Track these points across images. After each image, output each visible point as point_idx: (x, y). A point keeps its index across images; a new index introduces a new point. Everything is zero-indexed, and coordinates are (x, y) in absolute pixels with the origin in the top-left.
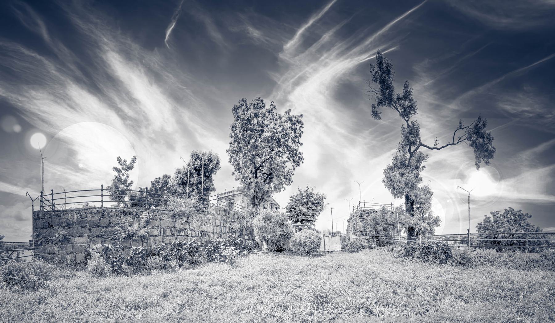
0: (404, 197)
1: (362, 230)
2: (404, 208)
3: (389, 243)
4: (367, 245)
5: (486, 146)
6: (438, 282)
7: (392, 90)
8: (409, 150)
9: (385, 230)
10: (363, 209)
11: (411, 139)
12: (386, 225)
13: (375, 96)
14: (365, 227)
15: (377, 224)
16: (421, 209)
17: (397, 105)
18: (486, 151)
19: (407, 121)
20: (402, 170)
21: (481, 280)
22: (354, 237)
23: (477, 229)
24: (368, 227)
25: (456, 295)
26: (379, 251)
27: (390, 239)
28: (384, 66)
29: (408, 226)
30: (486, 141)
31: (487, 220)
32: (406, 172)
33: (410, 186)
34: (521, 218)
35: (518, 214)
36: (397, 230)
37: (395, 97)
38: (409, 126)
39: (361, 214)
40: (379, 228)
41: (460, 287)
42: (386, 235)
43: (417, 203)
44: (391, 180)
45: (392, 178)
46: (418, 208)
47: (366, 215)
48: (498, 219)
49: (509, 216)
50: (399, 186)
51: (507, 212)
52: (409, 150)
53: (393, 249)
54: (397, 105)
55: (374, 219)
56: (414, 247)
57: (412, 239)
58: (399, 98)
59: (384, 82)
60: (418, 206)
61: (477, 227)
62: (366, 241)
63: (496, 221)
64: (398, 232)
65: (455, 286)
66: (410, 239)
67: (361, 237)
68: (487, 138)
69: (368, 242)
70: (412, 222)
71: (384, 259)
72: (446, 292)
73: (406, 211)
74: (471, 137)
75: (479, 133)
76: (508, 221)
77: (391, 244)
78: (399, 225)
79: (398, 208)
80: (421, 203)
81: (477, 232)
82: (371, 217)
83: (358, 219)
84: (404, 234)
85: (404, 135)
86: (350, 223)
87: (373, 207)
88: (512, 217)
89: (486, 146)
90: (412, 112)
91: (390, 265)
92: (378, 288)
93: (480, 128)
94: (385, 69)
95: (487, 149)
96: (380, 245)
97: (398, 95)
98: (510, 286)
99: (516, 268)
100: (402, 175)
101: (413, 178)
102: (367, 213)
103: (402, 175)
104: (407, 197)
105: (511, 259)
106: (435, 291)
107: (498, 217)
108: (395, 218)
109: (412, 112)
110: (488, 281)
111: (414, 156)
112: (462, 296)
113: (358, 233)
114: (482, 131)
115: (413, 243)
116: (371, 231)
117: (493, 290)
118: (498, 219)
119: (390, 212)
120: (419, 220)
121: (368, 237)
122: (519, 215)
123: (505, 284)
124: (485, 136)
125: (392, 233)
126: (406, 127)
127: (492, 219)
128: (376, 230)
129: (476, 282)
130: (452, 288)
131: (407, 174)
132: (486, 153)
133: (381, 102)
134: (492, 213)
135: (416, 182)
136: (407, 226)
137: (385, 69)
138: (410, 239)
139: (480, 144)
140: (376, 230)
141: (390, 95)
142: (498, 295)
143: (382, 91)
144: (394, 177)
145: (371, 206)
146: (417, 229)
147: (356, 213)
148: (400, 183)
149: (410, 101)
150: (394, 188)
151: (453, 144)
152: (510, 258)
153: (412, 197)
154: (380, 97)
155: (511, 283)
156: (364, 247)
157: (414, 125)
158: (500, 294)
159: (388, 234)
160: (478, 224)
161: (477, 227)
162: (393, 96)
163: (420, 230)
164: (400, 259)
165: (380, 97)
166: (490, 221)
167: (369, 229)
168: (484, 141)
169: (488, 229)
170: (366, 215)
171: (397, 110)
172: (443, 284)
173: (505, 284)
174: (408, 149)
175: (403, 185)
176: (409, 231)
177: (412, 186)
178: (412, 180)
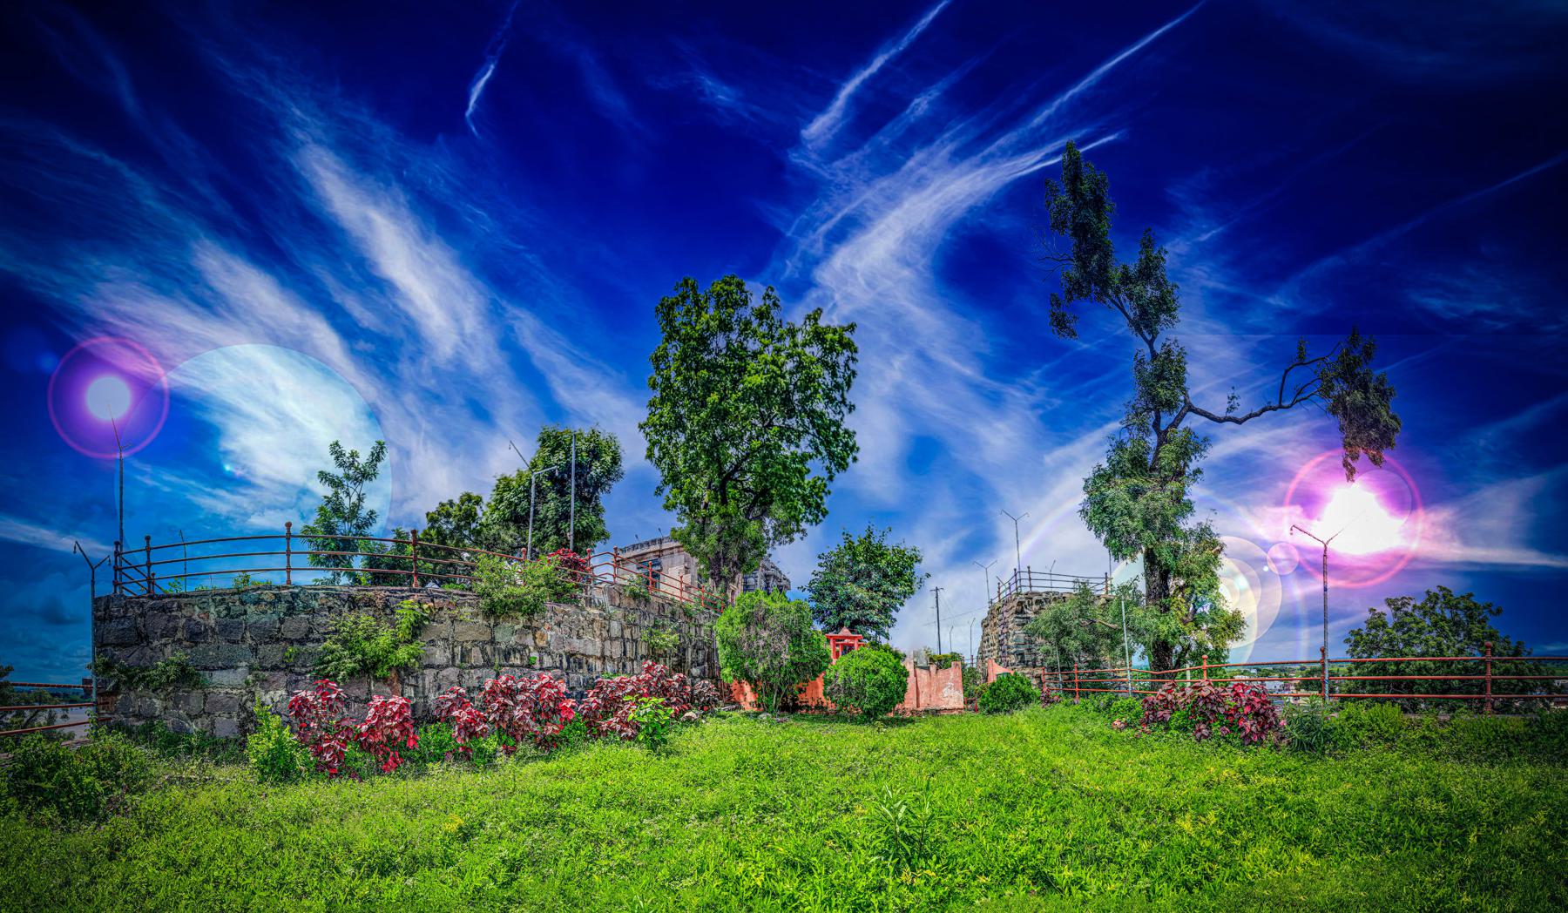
0: (1140, 556)
1: (1022, 649)
2: (1142, 587)
3: (1099, 687)
4: (1038, 692)
8: (1156, 425)
9: (1087, 648)
10: (1024, 590)
12: (1091, 637)
14: (1031, 642)
15: (1065, 632)
16: (1188, 591)
18: (1372, 426)
22: (1000, 670)
23: (1347, 647)
24: (1040, 640)
26: (1069, 713)
27: (1102, 676)
30: (1374, 400)
32: (1147, 485)
36: (1123, 649)
38: (1154, 356)
41: (1299, 812)
42: (1090, 665)
43: (1179, 574)
45: (1108, 503)
46: (1181, 589)
48: (1408, 619)
52: (1156, 425)
53: (1109, 705)
54: (1122, 296)
56: (1170, 697)
57: (1163, 676)
58: (1129, 278)
60: (1182, 583)
62: (1034, 681)
63: (1400, 626)
64: (1123, 656)
65: (1287, 809)
66: (1158, 677)
68: (1377, 390)
69: (1041, 684)
70: (1164, 628)
72: (1260, 826)
73: (1148, 596)
74: (1331, 388)
76: (1435, 624)
77: (1106, 688)
78: (1126, 638)
79: (1124, 589)
82: (1047, 614)
84: (1140, 660)
86: (988, 630)
88: (1448, 614)
90: (1163, 317)
93: (1357, 364)
94: (1089, 197)
95: (1377, 421)
96: (1073, 693)
98: (1441, 808)
99: (1458, 756)
100: (1136, 493)
102: (1038, 602)
103: (1136, 493)
104: (1150, 557)
107: (1406, 614)
109: (1163, 317)
110: (1377, 796)
111: (1169, 442)
112: (1306, 838)
113: (1013, 659)
116: (1047, 653)
118: (1408, 619)
119: (1103, 601)
121: (1039, 671)
123: (1427, 802)
126: (1148, 358)
127: (1390, 620)
128: (1062, 651)
130: (1278, 814)
134: (1390, 602)
135: (1175, 515)
136: (1150, 638)
138: (1158, 677)
139: (1356, 408)
143: (1079, 258)
144: (1112, 499)
153: (1165, 556)
156: (1027, 698)
157: (1168, 352)
158: (1412, 832)
159: (1099, 662)
161: (1347, 641)
163: (1186, 649)
164: (1129, 732)
166: (1384, 625)
168: (1367, 398)
169: (1378, 648)
172: (1250, 804)
173: (1426, 804)
174: (1151, 421)
176: (1156, 653)
177: (1163, 525)
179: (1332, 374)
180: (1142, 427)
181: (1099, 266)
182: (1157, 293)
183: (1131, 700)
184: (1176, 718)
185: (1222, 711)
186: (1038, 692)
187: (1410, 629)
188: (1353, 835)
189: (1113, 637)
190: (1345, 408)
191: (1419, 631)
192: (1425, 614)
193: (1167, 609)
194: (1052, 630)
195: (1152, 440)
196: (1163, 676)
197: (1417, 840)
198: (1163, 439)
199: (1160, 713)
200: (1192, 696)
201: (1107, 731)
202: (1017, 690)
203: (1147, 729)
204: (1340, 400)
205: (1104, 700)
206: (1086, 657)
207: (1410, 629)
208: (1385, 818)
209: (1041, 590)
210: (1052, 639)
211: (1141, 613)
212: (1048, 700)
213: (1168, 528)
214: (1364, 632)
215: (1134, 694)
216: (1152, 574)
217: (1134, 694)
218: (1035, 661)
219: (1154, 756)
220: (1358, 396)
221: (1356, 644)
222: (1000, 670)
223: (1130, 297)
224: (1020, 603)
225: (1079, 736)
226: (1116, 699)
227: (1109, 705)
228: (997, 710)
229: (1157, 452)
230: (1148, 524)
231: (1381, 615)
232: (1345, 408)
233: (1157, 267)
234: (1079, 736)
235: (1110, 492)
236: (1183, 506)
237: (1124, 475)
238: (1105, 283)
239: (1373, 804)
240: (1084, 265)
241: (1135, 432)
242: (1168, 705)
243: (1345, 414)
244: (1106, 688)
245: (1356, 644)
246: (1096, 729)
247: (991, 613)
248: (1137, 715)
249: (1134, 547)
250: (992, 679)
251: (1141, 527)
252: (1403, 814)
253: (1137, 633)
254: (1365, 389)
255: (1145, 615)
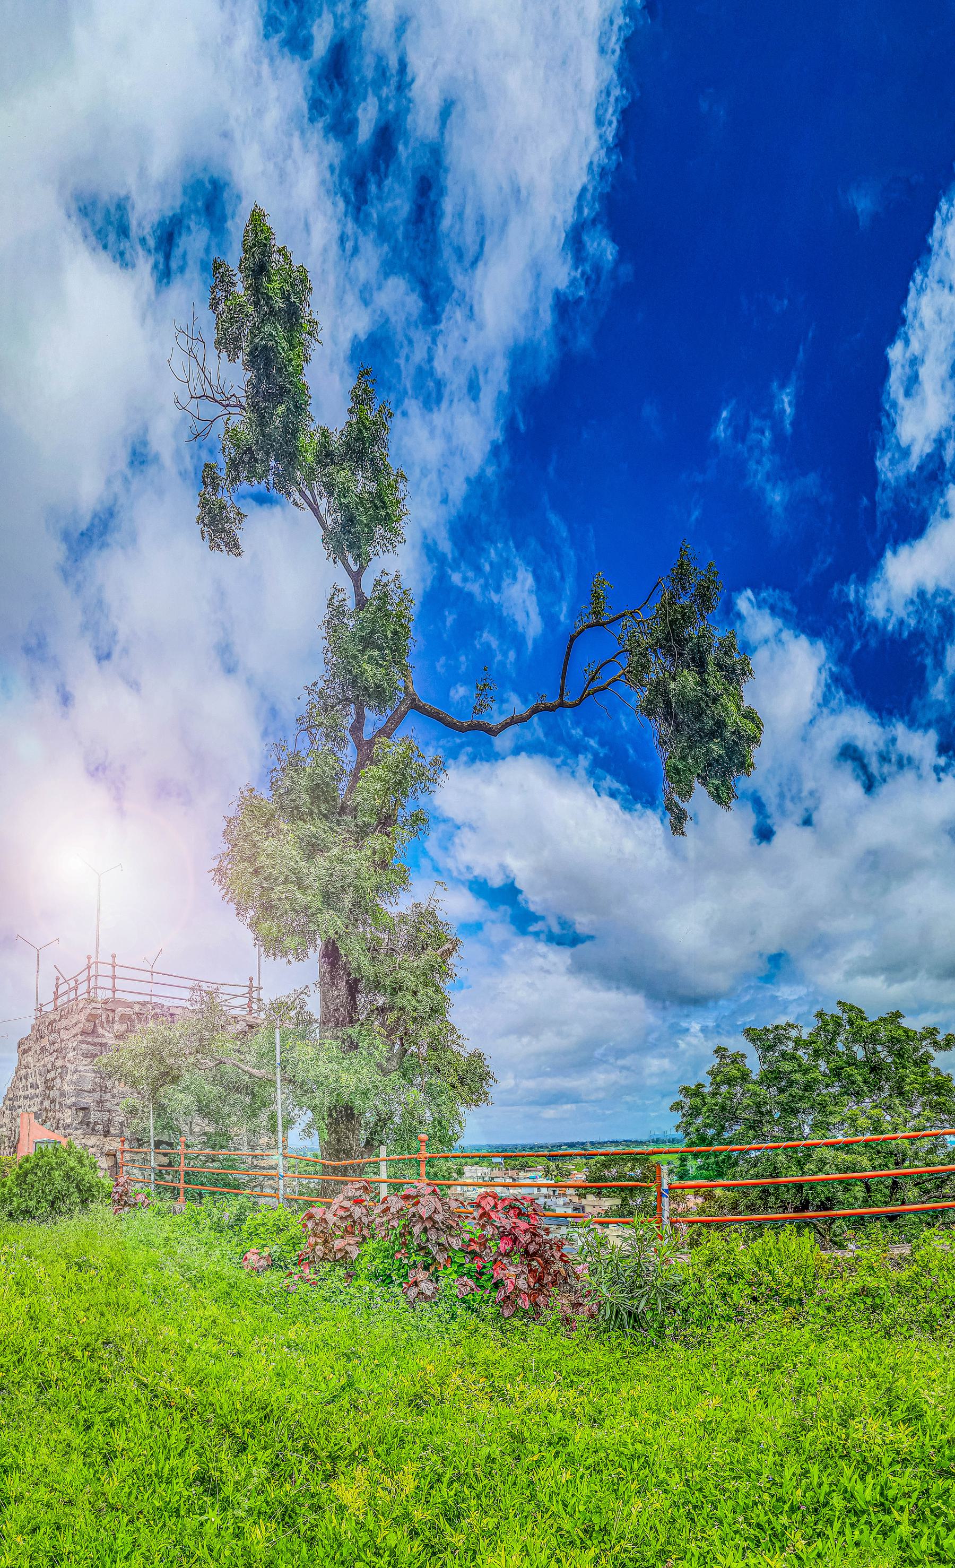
0: (315, 954)
1: (87, 1100)
2: (314, 1006)
3: (225, 1185)
4: (108, 1182)
5: (717, 710)
6: (470, 1429)
7: (299, 408)
8: (357, 729)
9: (205, 1111)
10: (102, 995)
11: (369, 670)
12: (216, 1090)
13: (219, 428)
14: (105, 1090)
15: (169, 1076)
16: (392, 1017)
17: (317, 486)
18: (712, 734)
19: (356, 578)
20: (314, 828)
21: (738, 1411)
22: (42, 1133)
23: (677, 1117)
24: (121, 1088)
25: (567, 1524)
26: (167, 1226)
27: (231, 1164)
28: (274, 286)
29: (327, 1101)
30: (716, 684)
31: (728, 1072)
32: (331, 838)
33: (347, 902)
34: (900, 1055)
35: (883, 1036)
36: (273, 1117)
37: (309, 445)
38: (361, 602)
39: (92, 1018)
40: (179, 1100)
41: (596, 1469)
42: (211, 1141)
43: (377, 985)
44: (256, 872)
45: (262, 860)
46: (382, 1011)
47: (119, 1027)
48: (786, 1066)
49: (840, 1047)
50: (293, 901)
51: (829, 1027)
52: (357, 729)
53: (239, 1219)
54: (317, 486)
55: (155, 1053)
56: (358, 1212)
57: (345, 1171)
58: (329, 454)
59: (268, 363)
60: (380, 1001)
61: (677, 1107)
62: (104, 1163)
63: (773, 1077)
64: (273, 1129)
65: (571, 1460)
66: (336, 1171)
67: (79, 1140)
68: (720, 666)
69: (116, 1168)
70: (348, 1079)
71: (185, 1269)
72: (512, 1500)
73: (324, 1022)
74: (645, 667)
75: (681, 642)
76: (837, 1072)
77: (236, 1187)
78: (280, 1095)
79: (280, 1008)
80: (397, 989)
81: (680, 1134)
82: (137, 1042)
83: (71, 1040)
84: (303, 1139)
85: (338, 648)
86: (29, 1059)
87: (158, 990)
88: (859, 1053)
89: (717, 710)
90: (379, 531)
91: (213, 1310)
92: (119, 1440)
93: (686, 619)
94: (279, 303)
95: (720, 725)
96: (175, 1193)
97: (325, 434)
98: (904, 1438)
99: (929, 1325)
100: (313, 848)
101: (365, 867)
102: (124, 1018)
103: (313, 848)
104: (332, 954)
105: (904, 1275)
106: (444, 1493)
107: (784, 1055)
108: (266, 1055)
109: (379, 531)
110: (773, 1420)
111: (375, 762)
112: (605, 1531)
113: (68, 1117)
114: (692, 632)
115: (351, 1190)
116: (133, 1111)
117: (805, 1473)
118: (786, 1066)
119: (242, 1026)
120: (386, 1073)
121: (114, 1145)
122: (893, 1040)
123: (874, 1426)
124: (711, 658)
125: (240, 1131)
126: (350, 604)
127: (754, 1064)
128: (161, 1110)
129: (709, 1428)
130: (554, 1473)
131: (335, 851)
132: (716, 749)
133: (244, 461)
134: (753, 1035)
135: (377, 888)
136: (323, 1099)
137: (279, 303)
138: (336, 1171)
139: (686, 704)
140: (161, 1110)
141: (291, 432)
142: (837, 1501)
143: (255, 407)
144: (271, 856)
145: (146, 988)
146: (370, 1117)
147: (66, 1015)
148: (300, 884)
149: (378, 470)
150: (267, 908)
151: (562, 705)
152: (894, 1274)
153: (356, 955)
154: (248, 436)
155: (907, 1421)
156: (86, 1195)
157: (384, 598)
158: (848, 1495)
159: (224, 1135)
160: (685, 1091)
161: (677, 1107)
162: (303, 440)
163: (383, 1121)
164: (273, 1277)
165: (248, 436)
166: (745, 1077)
167: (124, 1098)
168: (704, 683)
169: (735, 1119)
170: (119, 1027)
171: (316, 511)
172: (495, 1450)
173: (872, 1431)
174: (349, 721)
175: (312, 898)
176: (333, 1126)
177: (356, 904)
178: (358, 875)
179: (646, 640)
180: (333, 732)
181: (286, 427)
182: (373, 487)
183: (282, 1212)
184: (368, 1256)
185: (456, 1243)
186: (108, 1182)
187: (791, 1084)
188: (725, 1510)
189: (254, 1095)
190: (668, 704)
191: (808, 1088)
192: (817, 1054)
193: (354, 1046)
194: (146, 1071)
195: (349, 755)
196: (345, 1171)
197: (858, 1513)
198: (366, 756)
199: (338, 1244)
200: (400, 1214)
201: (229, 1271)
202: (67, 1177)
203: (309, 1273)
204: (660, 688)
205: (231, 1209)
206: (202, 1126)
207: (791, 1084)
208: (792, 1468)
209: (131, 998)
210: (145, 1087)
211: (311, 1052)
212: (122, 1201)
213: (363, 909)
214: (707, 1090)
215: (289, 1201)
216: (333, 984)
217: (289, 1201)
218: (109, 1123)
219: (317, 1333)
220: (690, 678)
221: (695, 1112)
222: (42, 1133)
223: (330, 488)
224: (92, 1018)
225: (171, 1276)
226: (255, 1208)
227: (239, 1219)
228: (27, 1213)
229: (356, 778)
230: (329, 899)
231: (737, 1059)
232: (668, 704)
233: (375, 440)
234: (171, 1276)
235: (269, 845)
236: (493, 542)
237: (296, 814)
238: (291, 457)
239: (767, 1440)
240: (262, 420)
241: (320, 741)
242: (352, 1227)
243: (669, 714)
244: (236, 1187)
245: (695, 1112)
246: (209, 1267)
247: (37, 1028)
248: (294, 1242)
249: (307, 937)
250: (26, 1149)
251: (318, 903)
252: (828, 1456)
253: (300, 1087)
254: (700, 665)
255: (318, 1057)
